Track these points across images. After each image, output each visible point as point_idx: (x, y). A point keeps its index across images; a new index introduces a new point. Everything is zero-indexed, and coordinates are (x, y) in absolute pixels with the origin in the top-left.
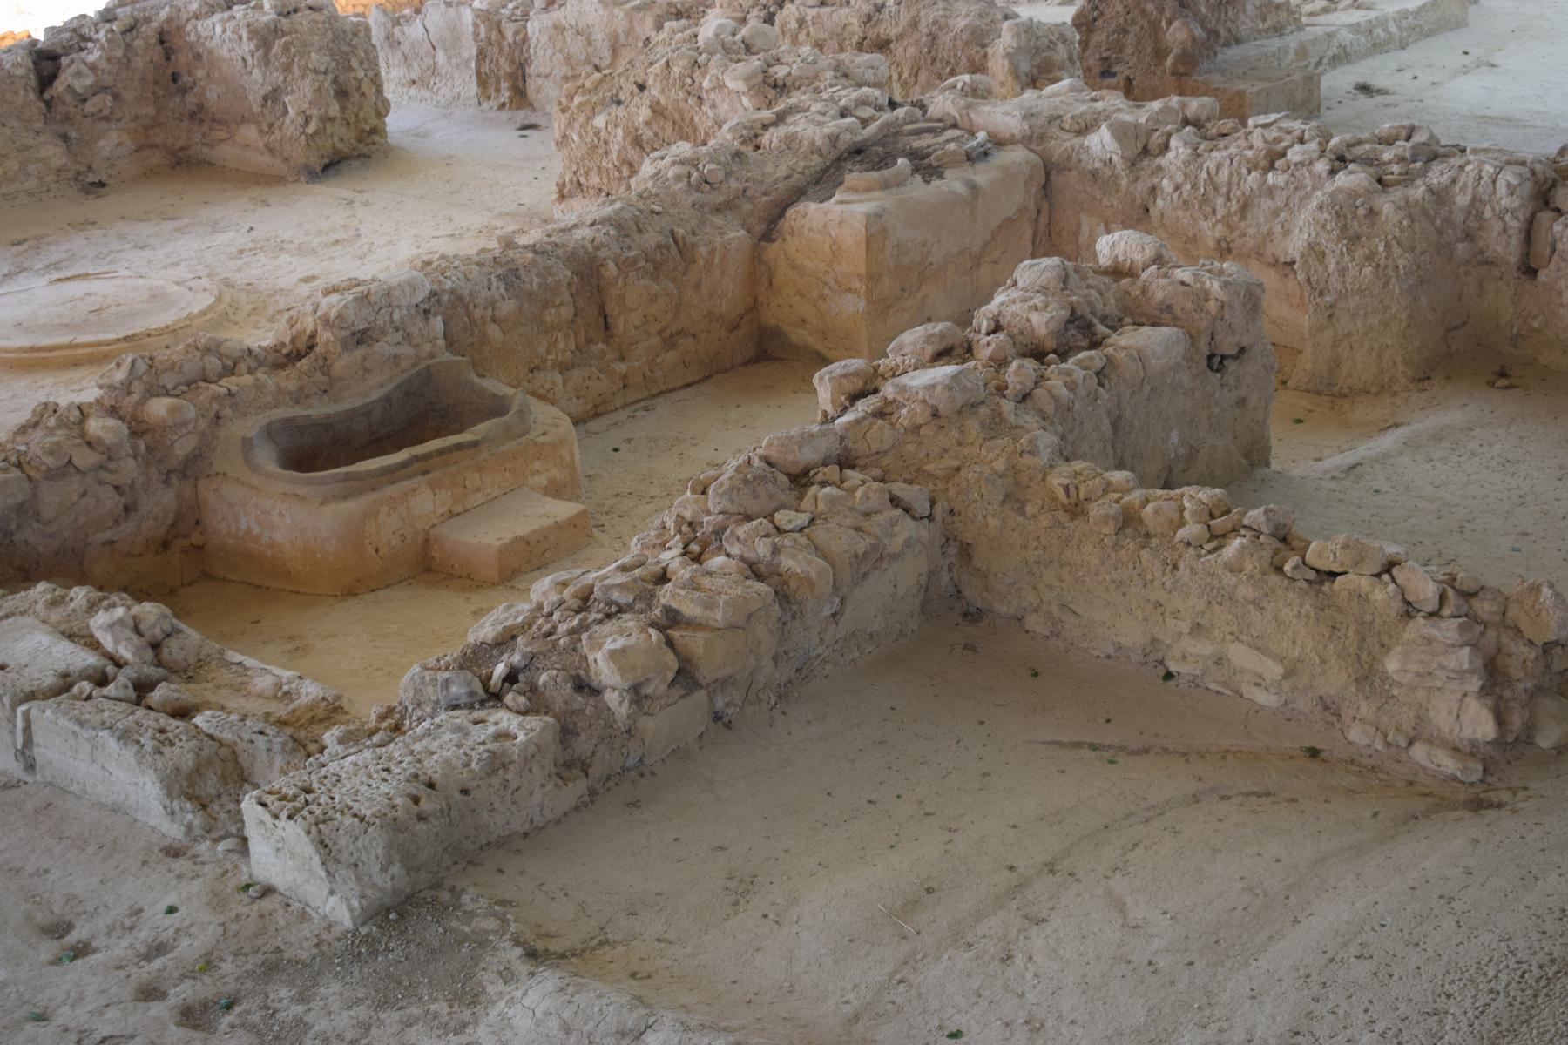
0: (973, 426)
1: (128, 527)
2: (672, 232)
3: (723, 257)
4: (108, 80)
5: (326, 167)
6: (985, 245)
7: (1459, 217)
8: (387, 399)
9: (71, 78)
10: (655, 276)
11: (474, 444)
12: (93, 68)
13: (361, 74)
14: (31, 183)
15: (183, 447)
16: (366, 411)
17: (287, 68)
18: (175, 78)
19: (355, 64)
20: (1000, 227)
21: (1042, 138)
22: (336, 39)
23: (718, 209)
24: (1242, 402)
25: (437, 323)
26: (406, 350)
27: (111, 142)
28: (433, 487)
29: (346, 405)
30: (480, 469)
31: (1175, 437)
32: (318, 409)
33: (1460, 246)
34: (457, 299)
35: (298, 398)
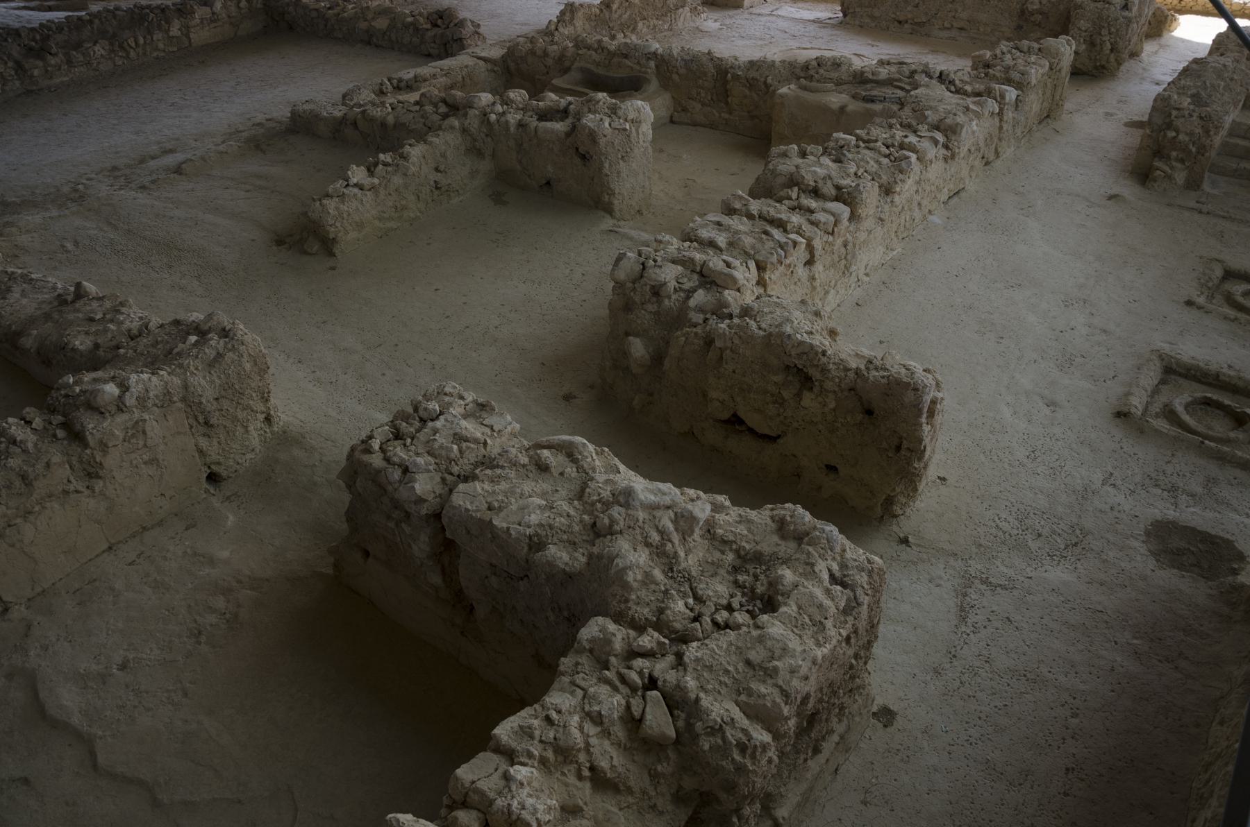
19: (1104, 32)
25: (652, 64)
26: (638, 67)
32: (601, 71)
35: (598, 64)
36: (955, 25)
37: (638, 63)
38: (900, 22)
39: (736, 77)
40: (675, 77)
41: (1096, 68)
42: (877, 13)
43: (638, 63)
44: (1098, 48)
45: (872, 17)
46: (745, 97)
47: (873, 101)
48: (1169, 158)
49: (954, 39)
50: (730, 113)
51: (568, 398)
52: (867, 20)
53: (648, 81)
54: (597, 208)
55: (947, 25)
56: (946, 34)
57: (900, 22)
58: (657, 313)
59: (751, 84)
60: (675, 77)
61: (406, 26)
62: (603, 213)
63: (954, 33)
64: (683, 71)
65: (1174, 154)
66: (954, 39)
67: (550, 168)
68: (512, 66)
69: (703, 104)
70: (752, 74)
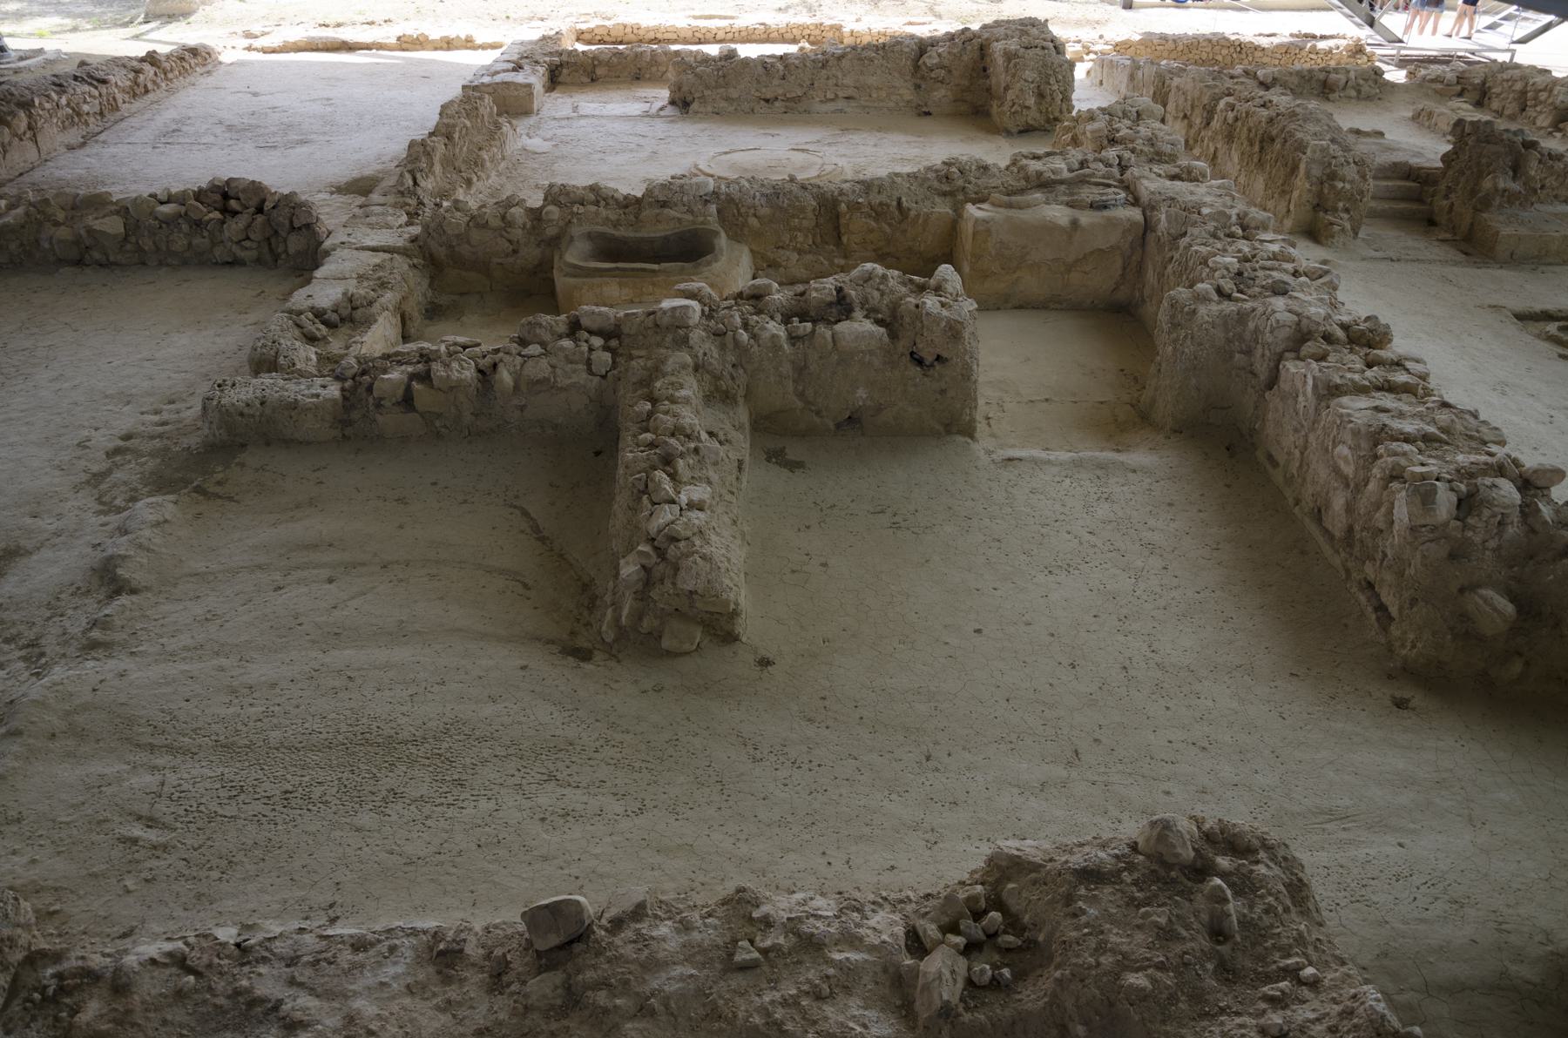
0: (669, 338)
1: (511, 260)
2: (899, 199)
3: (926, 221)
4: (946, 62)
5: (1021, 132)
6: (1077, 261)
7: (1247, 336)
8: (666, 238)
9: (931, 59)
10: (876, 220)
11: (653, 271)
12: (939, 55)
13: (1055, 87)
14: (892, 104)
15: (551, 231)
16: (651, 241)
17: (1014, 76)
18: (985, 70)
19: (1052, 81)
20: (1092, 253)
21: (1153, 208)
22: (1045, 65)
23: (944, 194)
24: (943, 392)
25: (713, 208)
26: (689, 217)
27: (940, 94)
28: (620, 285)
29: (643, 234)
30: (654, 284)
31: (861, 393)
32: (622, 232)
33: (1237, 356)
34: (730, 199)
35: (616, 225)
36: (841, 94)
37: (690, 211)
38: (767, 101)
39: (855, 207)
40: (753, 221)
41: (1048, 121)
42: (734, 94)
43: (690, 211)
44: (1048, 99)
45: (728, 99)
46: (871, 231)
47: (1105, 207)
48: (1335, 210)
49: (841, 111)
50: (846, 257)
51: (1401, 704)
52: (723, 104)
53: (716, 233)
54: (948, 432)
55: (830, 95)
56: (830, 106)
57: (767, 101)
58: (1499, 547)
59: (878, 212)
60: (753, 221)
61: (169, 222)
62: (960, 439)
63: (840, 104)
64: (765, 211)
65: (1341, 205)
66: (841, 111)
67: (861, 393)
68: (441, 252)
69: (800, 252)
70: (876, 199)
